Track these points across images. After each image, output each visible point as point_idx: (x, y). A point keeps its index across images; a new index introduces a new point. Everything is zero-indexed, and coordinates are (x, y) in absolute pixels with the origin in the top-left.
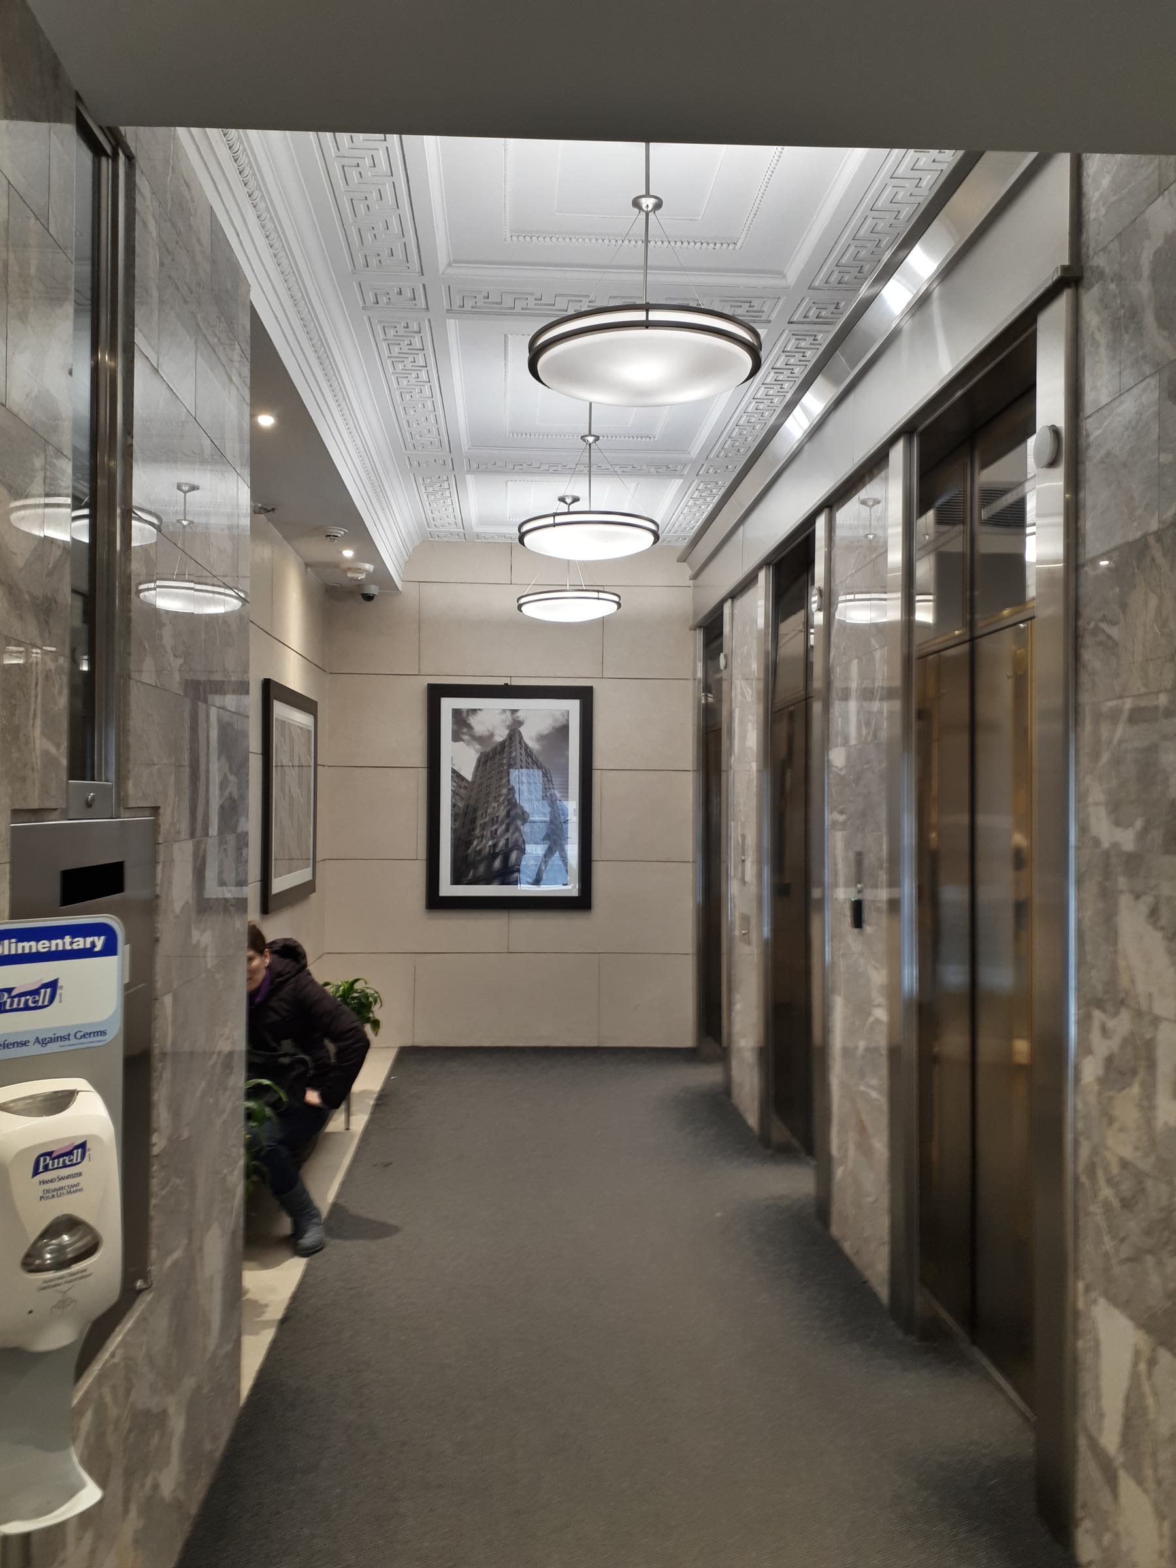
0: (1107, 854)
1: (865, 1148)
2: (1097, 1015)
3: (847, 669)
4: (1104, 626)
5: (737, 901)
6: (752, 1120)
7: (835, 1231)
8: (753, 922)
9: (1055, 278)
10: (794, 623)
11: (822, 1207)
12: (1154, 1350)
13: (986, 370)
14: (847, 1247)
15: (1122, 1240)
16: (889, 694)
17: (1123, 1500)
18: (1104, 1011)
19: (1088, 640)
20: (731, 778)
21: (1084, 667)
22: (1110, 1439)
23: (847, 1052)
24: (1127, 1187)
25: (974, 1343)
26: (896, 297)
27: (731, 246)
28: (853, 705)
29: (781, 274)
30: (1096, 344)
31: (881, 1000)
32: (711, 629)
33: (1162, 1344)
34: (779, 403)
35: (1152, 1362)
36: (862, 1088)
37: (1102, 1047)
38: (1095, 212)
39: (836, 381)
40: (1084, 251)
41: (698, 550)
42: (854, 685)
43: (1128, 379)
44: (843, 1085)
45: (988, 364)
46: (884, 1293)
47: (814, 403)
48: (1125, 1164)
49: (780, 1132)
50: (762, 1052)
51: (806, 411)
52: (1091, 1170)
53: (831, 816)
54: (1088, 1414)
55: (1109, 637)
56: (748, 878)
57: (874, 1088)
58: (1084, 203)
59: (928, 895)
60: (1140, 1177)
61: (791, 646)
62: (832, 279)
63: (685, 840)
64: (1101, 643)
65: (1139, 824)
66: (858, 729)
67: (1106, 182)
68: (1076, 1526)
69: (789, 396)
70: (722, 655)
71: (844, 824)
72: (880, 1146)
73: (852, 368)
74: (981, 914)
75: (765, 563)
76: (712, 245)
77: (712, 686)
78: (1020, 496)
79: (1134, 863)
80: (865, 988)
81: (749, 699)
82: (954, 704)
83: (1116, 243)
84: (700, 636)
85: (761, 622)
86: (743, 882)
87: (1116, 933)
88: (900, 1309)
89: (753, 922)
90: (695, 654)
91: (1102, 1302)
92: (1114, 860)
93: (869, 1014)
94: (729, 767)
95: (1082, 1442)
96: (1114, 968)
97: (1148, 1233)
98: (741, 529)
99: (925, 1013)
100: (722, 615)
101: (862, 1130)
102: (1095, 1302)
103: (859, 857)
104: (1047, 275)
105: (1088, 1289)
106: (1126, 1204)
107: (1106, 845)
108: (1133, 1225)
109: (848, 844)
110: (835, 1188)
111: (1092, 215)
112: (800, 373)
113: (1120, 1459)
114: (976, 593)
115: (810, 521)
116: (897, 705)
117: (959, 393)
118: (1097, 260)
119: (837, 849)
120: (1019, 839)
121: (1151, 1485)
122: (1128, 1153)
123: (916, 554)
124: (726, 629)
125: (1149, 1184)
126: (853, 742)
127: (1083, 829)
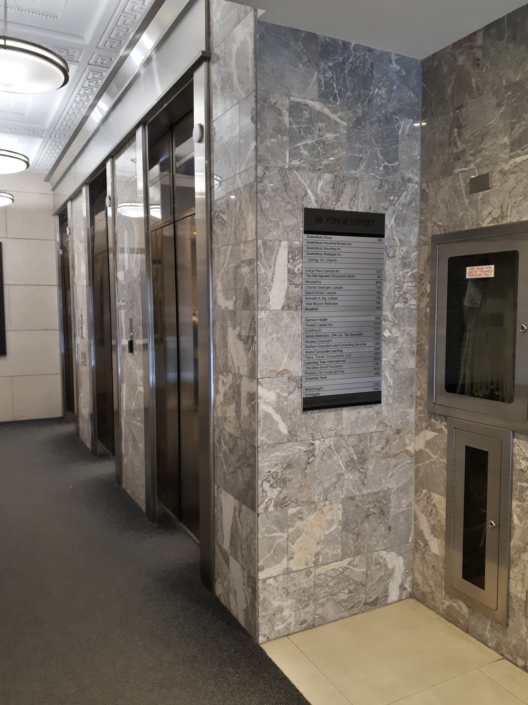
0: (223, 311)
1: (135, 448)
2: (221, 377)
3: (123, 234)
4: (221, 214)
5: (80, 346)
6: (89, 445)
7: (124, 486)
8: (87, 355)
9: (199, 56)
10: (99, 217)
11: (118, 478)
12: (240, 507)
13: (176, 95)
14: (129, 492)
15: (230, 466)
16: (141, 251)
17: (231, 567)
18: (223, 375)
19: (215, 221)
20: (75, 288)
21: (214, 232)
22: (226, 546)
23: (128, 411)
24: (231, 445)
25: (180, 521)
26: (137, 57)
27: (55, 19)
28: (126, 256)
29: (82, 38)
30: (216, 88)
31: (142, 383)
32: (62, 216)
33: (243, 503)
34: (88, 104)
35: (240, 511)
36: (134, 422)
37: (222, 389)
38: (215, 28)
39: (112, 96)
40: (211, 45)
41: (54, 176)
42: (126, 246)
43: (228, 106)
44: (126, 422)
45: (176, 93)
46: (143, 507)
47: (104, 105)
48: (230, 435)
49: (101, 447)
50: (92, 416)
51: (100, 109)
52: (219, 441)
53: (119, 303)
54: (219, 536)
55: (223, 219)
56: (84, 335)
57: (139, 422)
58: (211, 23)
59: (160, 342)
60: (235, 439)
61: (100, 226)
62: (107, 45)
63: (55, 320)
64: (220, 222)
65: (234, 298)
66: (129, 266)
67: (219, 14)
68: (215, 582)
69: (91, 102)
70: (67, 228)
71: (124, 306)
72: (142, 446)
73: (119, 91)
74: (182, 353)
75: (85, 183)
76: (45, 16)
77: (64, 247)
78: (192, 156)
79: (233, 313)
80: (135, 376)
81: (81, 249)
82: (168, 257)
83: (223, 43)
84: (57, 219)
85: (85, 213)
86: (83, 337)
87: (227, 343)
88: (151, 515)
89: (87, 355)
90: (55, 229)
91: (223, 491)
92: (226, 314)
93: (137, 389)
94: (74, 283)
95: (217, 548)
96: (227, 357)
97: (238, 461)
98: (74, 167)
99: (160, 392)
100: (66, 209)
101: (134, 439)
102: (221, 492)
103: (131, 321)
104: (196, 55)
105: (218, 487)
106: (231, 451)
107: (223, 308)
108: (233, 458)
109: (126, 315)
110: (124, 467)
111: (214, 29)
112: (96, 90)
113: (230, 551)
114: (175, 205)
115: (103, 164)
116: (144, 256)
117: (165, 105)
118: (216, 50)
119: (122, 317)
120: (195, 319)
121: (240, 558)
122: (231, 430)
123: (149, 185)
124: (69, 216)
125: (239, 442)
126: (127, 268)
127: (215, 302)
